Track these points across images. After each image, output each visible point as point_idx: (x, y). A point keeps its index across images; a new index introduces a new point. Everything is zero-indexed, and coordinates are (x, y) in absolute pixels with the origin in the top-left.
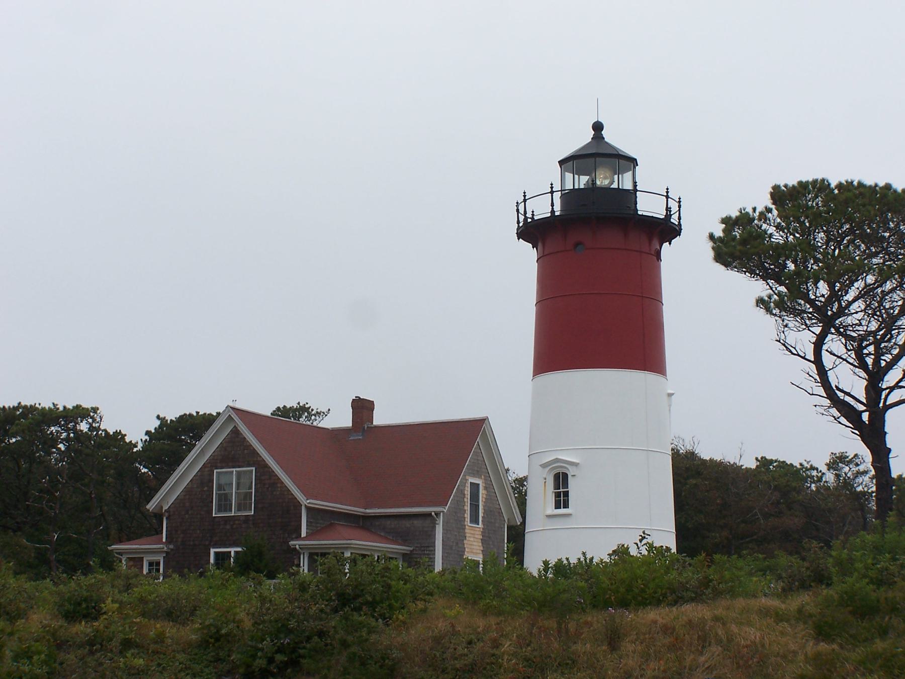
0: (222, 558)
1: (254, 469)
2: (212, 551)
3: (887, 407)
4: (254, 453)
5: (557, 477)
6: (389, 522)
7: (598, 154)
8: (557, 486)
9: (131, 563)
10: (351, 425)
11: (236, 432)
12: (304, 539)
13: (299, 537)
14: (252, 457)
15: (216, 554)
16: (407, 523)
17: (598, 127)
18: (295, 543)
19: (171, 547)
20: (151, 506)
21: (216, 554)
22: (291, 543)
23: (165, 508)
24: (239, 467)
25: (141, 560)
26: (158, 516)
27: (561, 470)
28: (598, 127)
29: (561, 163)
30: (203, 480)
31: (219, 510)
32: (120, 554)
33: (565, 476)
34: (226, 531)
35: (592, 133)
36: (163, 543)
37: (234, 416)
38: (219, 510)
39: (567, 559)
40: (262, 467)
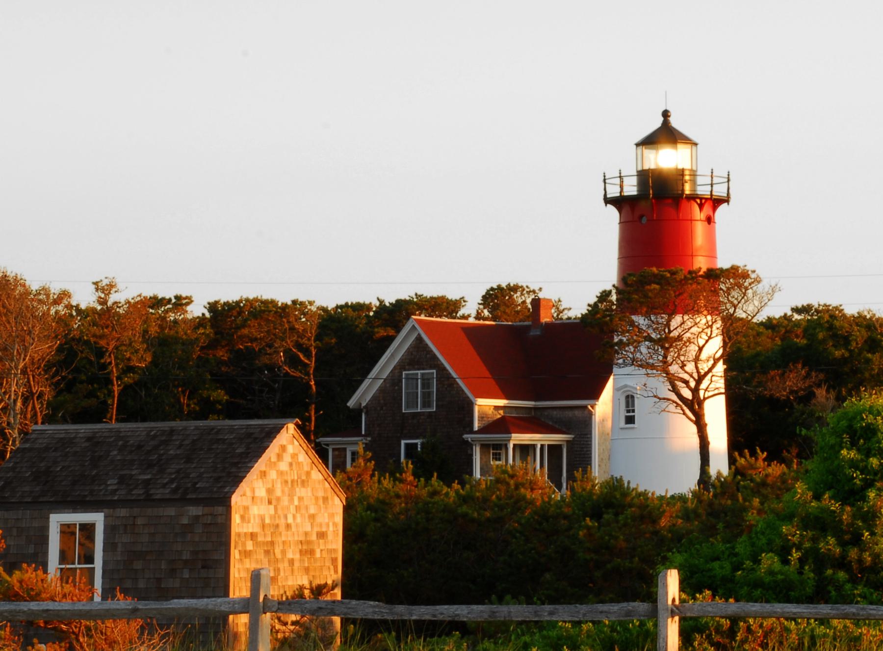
0: (410, 448)
1: (56, 520)
2: (403, 442)
3: (705, 399)
4: (435, 357)
5: (627, 397)
6: (555, 413)
7: (666, 134)
8: (627, 405)
9: (337, 453)
10: (51, 515)
11: (419, 339)
12: (476, 433)
13: (472, 432)
14: (432, 362)
15: (407, 445)
16: (569, 414)
17: (666, 114)
18: (468, 437)
19: (369, 439)
20: (351, 403)
21: (407, 445)
22: (465, 436)
23: (364, 404)
24: (423, 369)
25: (345, 449)
26: (357, 413)
27: (630, 393)
28: (666, 114)
29: (638, 145)
30: (394, 381)
31: (88, 530)
32: (327, 445)
33: (633, 397)
34: (410, 425)
35: (662, 119)
36: (362, 436)
37: (417, 326)
38: (407, 407)
39: (629, 482)
40: (441, 369)
